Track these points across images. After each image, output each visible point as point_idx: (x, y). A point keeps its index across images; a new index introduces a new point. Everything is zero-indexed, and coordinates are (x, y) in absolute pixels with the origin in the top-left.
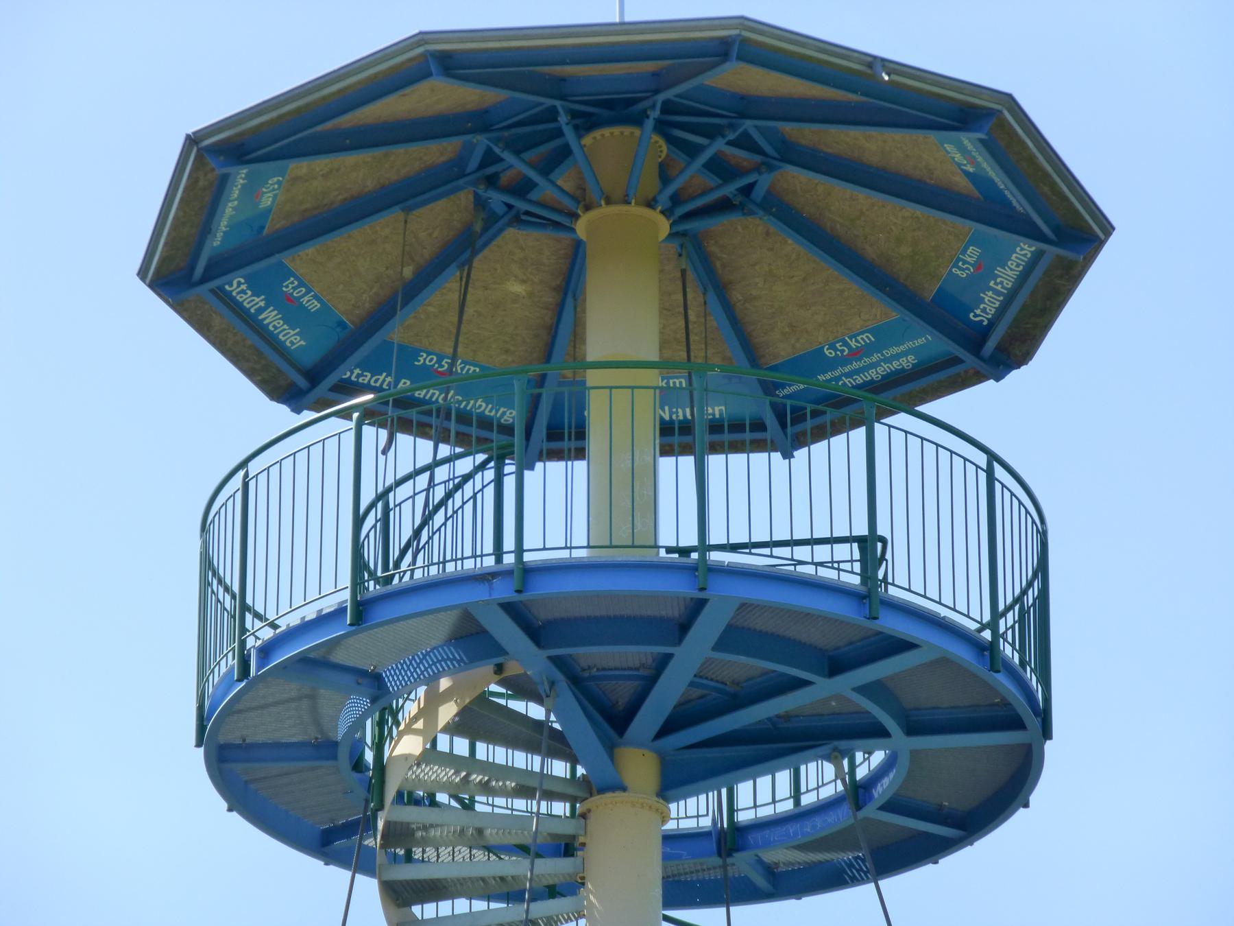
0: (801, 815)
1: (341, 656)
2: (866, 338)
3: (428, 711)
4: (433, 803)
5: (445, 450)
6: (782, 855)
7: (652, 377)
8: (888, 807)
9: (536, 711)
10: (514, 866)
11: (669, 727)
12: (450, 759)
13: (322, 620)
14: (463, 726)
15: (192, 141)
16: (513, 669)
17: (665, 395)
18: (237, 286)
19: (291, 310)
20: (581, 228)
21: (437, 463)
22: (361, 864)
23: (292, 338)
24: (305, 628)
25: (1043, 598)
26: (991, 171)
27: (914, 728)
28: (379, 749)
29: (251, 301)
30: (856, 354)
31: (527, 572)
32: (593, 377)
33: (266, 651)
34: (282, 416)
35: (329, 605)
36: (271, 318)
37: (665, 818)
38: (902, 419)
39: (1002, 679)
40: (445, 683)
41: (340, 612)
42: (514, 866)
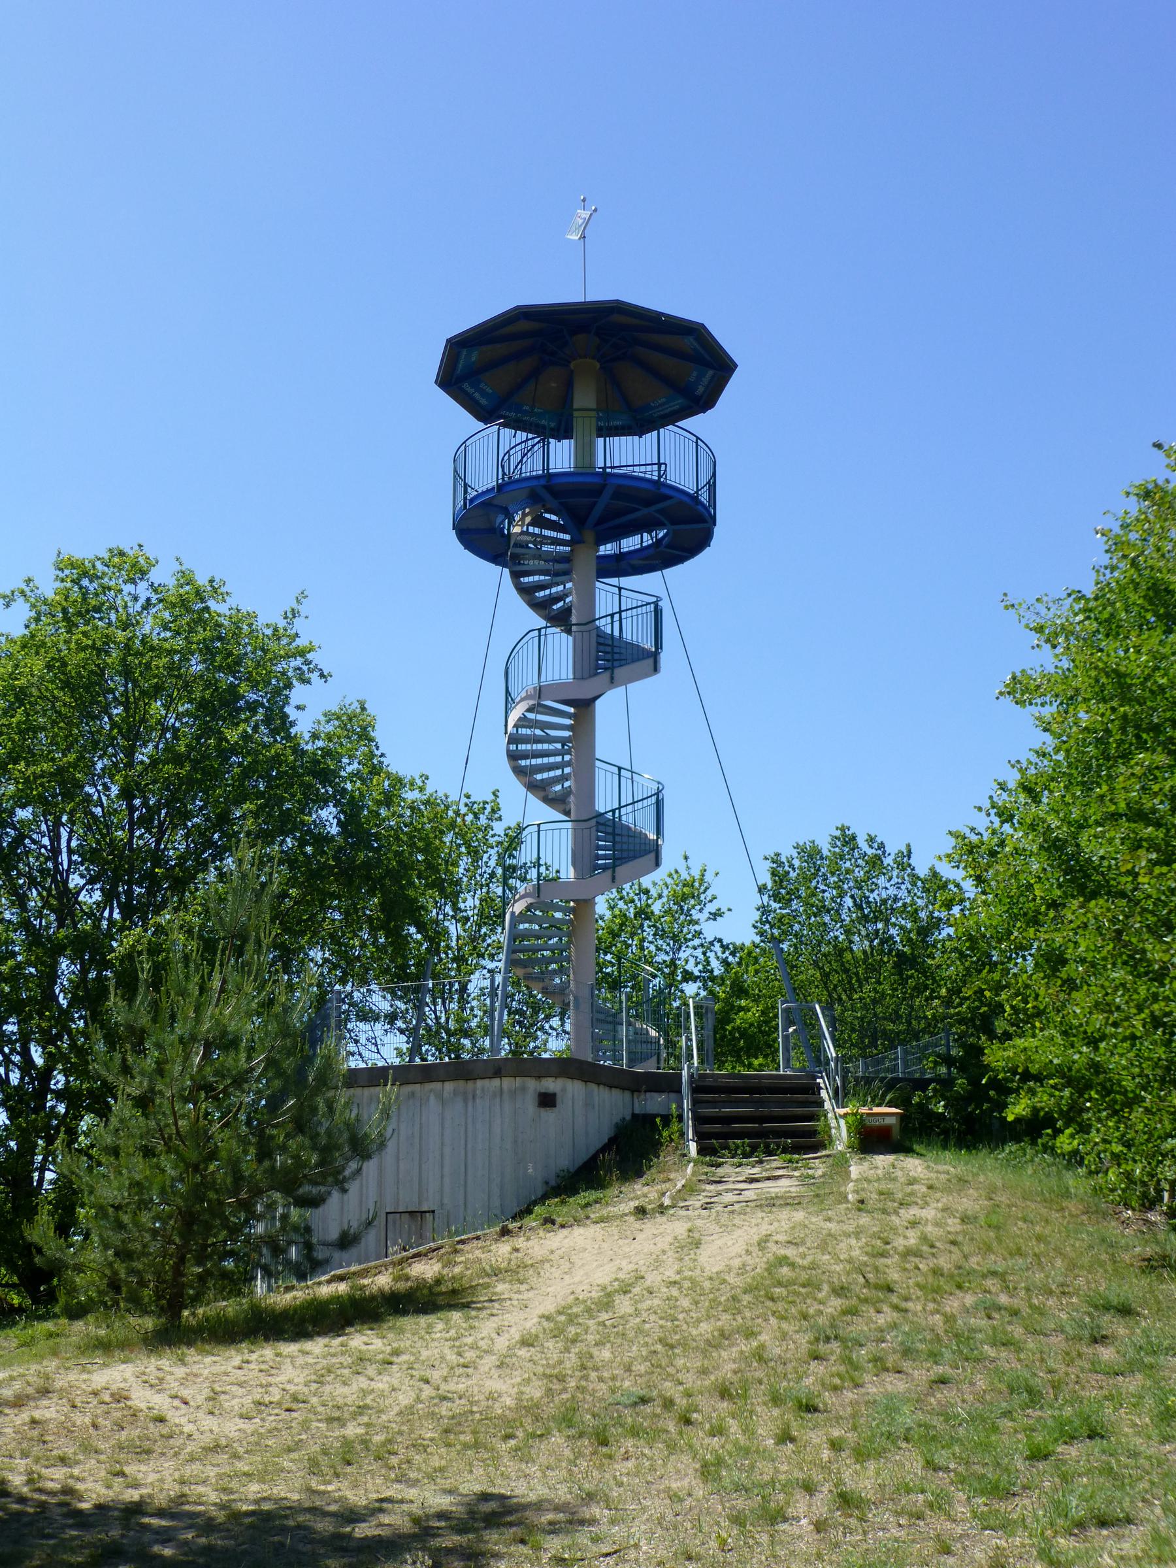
0: (642, 549)
1: (496, 502)
2: (664, 400)
3: (522, 519)
4: (528, 547)
5: (530, 436)
6: (635, 562)
7: (593, 414)
8: (667, 546)
9: (554, 518)
10: (550, 566)
11: (599, 522)
12: (533, 534)
13: (488, 491)
14: (533, 523)
15: (448, 341)
16: (548, 506)
17: (599, 419)
18: (466, 386)
19: (483, 393)
20: (572, 366)
21: (527, 440)
22: (504, 565)
23: (484, 402)
24: (483, 493)
25: (715, 483)
26: (695, 344)
27: (673, 523)
28: (509, 529)
29: (470, 390)
30: (661, 405)
31: (551, 476)
32: (576, 414)
33: (472, 501)
34: (481, 425)
35: (490, 486)
36: (477, 395)
37: (598, 551)
38: (671, 427)
39: (700, 507)
40: (527, 510)
41: (493, 488)
42: (550, 566)
